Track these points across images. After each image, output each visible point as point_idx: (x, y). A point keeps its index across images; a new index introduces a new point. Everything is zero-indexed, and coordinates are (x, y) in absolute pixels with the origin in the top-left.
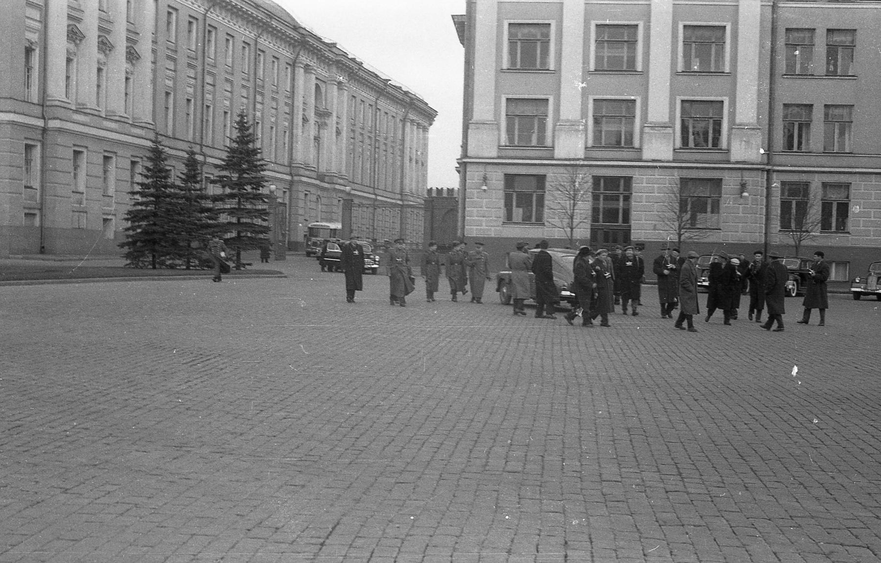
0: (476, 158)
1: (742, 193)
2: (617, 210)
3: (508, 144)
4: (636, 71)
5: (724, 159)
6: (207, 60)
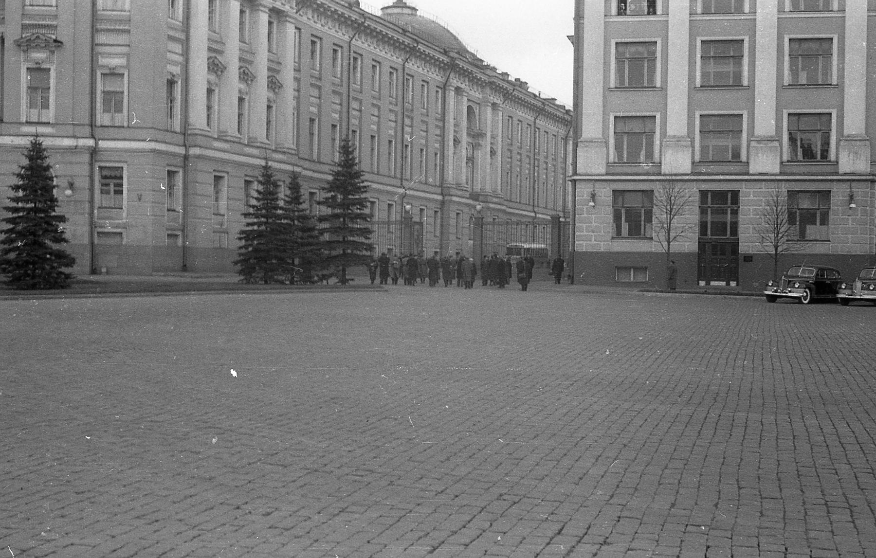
0: (585, 175)
1: (850, 204)
2: (725, 224)
3: (617, 161)
4: (742, 86)
5: (833, 171)
6: (353, 86)
